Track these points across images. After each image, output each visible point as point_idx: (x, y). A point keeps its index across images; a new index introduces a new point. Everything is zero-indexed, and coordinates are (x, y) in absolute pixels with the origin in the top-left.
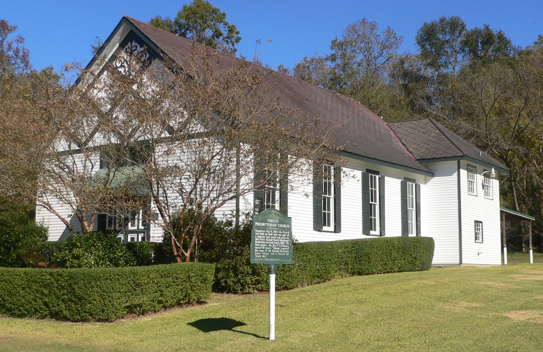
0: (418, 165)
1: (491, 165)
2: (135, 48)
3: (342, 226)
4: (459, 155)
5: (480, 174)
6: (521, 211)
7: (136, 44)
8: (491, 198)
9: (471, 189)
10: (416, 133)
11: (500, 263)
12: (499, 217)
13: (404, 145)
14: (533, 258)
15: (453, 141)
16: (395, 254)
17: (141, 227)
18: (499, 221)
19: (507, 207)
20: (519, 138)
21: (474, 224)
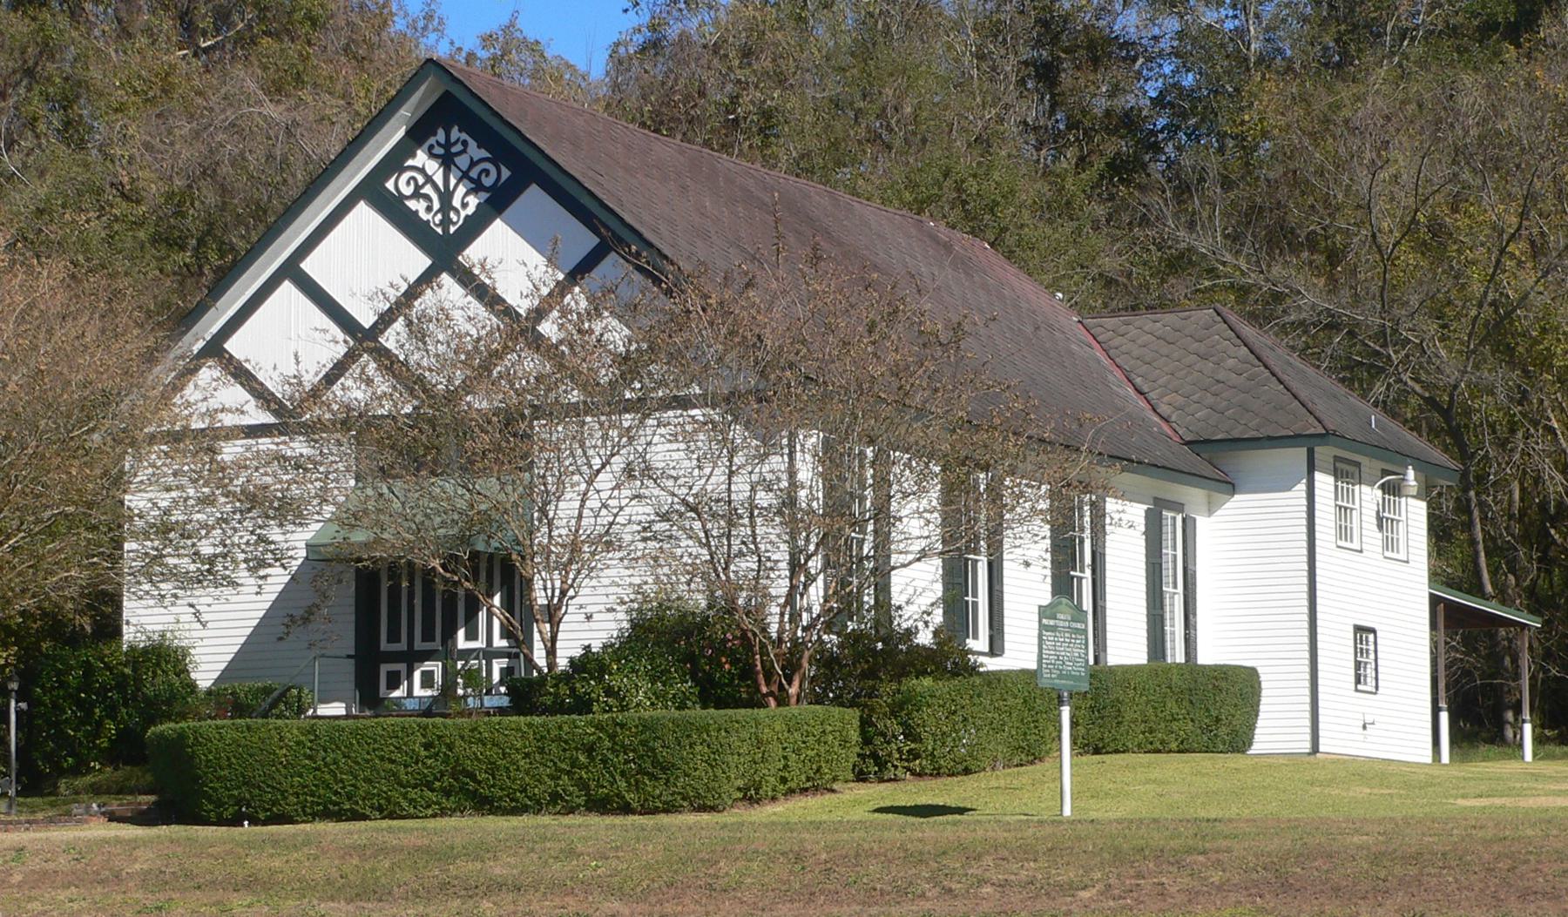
0: (1187, 459)
1: (1405, 457)
2: (459, 147)
3: (1006, 637)
4: (1312, 431)
5: (1372, 484)
6: (1503, 598)
7: (464, 136)
8: (1402, 556)
9: (1344, 532)
10: (1176, 355)
11: (1427, 757)
12: (1426, 615)
13: (1141, 393)
14: (1072, 766)
15: (1294, 385)
16: (1171, 704)
17: (499, 642)
18: (1427, 628)
19: (1451, 584)
20: (1499, 334)
21: (1351, 636)
